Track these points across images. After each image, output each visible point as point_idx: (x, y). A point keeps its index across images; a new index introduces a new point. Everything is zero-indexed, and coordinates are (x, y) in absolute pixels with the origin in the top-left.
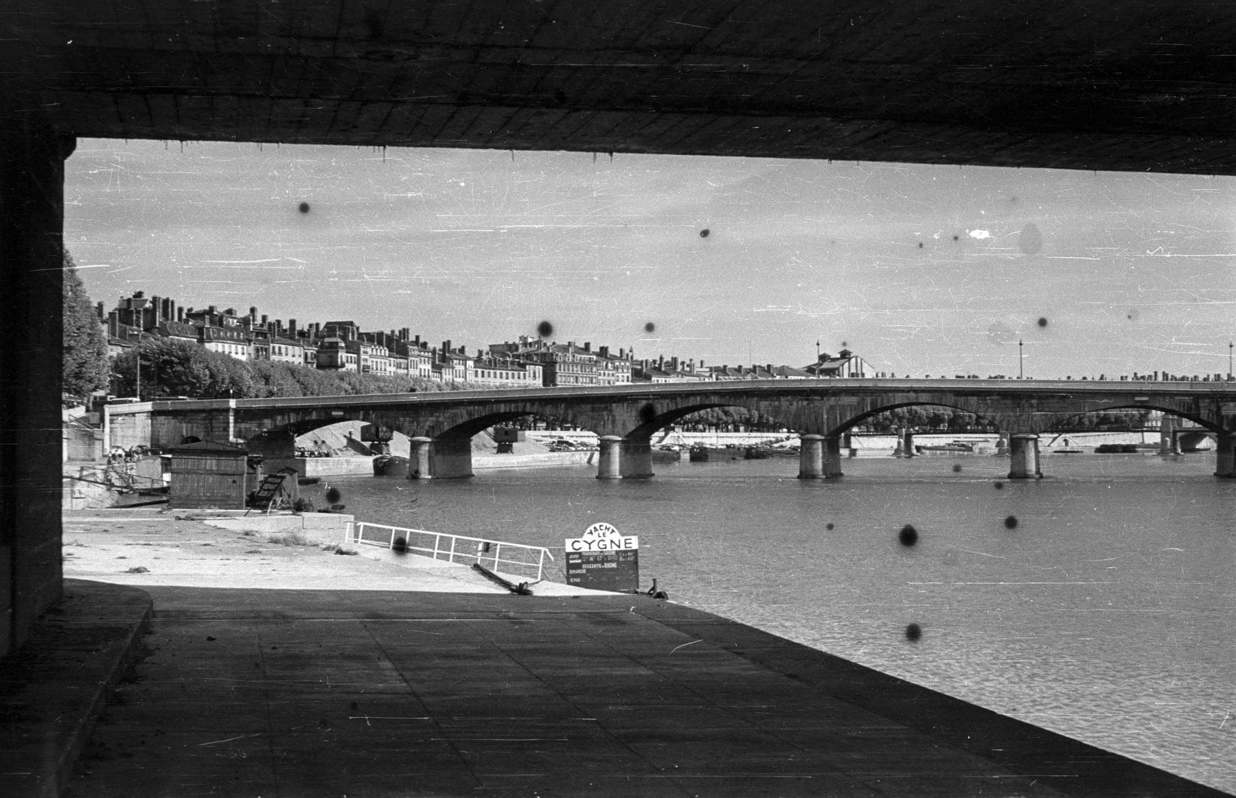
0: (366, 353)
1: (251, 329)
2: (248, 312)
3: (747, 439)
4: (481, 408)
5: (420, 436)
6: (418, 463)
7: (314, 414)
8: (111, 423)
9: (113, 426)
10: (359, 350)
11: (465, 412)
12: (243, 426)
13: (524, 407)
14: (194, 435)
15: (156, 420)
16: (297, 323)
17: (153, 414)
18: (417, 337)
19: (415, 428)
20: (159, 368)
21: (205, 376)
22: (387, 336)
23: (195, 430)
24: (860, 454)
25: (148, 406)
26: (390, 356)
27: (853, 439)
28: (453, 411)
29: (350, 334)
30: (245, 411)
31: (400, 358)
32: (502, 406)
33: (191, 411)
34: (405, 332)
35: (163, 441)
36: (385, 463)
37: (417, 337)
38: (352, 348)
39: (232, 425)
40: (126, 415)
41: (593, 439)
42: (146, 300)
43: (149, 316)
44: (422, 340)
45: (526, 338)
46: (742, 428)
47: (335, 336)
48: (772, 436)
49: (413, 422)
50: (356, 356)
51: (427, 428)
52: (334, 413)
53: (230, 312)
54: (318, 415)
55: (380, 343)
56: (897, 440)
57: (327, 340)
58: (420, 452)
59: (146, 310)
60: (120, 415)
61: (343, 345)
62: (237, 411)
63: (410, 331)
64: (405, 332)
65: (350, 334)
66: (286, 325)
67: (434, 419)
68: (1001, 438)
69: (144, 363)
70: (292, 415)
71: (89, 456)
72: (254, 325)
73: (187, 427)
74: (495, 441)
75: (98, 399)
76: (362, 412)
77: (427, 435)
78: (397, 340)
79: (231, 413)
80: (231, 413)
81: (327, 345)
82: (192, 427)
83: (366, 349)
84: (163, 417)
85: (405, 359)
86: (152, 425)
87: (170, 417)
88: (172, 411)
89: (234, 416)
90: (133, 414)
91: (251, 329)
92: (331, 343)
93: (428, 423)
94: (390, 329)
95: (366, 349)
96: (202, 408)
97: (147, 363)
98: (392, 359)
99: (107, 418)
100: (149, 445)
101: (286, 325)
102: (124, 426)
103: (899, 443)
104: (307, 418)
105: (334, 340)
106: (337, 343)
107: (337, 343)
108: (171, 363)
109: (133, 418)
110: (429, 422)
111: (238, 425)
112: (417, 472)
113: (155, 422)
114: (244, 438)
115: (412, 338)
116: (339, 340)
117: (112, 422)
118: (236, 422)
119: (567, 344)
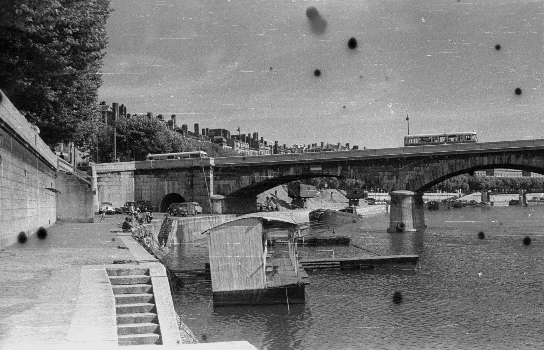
0: (237, 146)
1: (174, 129)
2: (170, 119)
3: (441, 197)
4: (463, 161)
5: (400, 189)
6: (401, 216)
7: (292, 169)
8: (98, 181)
9: (100, 183)
10: (233, 144)
11: (447, 166)
12: (222, 182)
13: (509, 159)
14: (175, 192)
15: (139, 178)
16: (199, 125)
17: (137, 173)
18: (262, 138)
19: (394, 181)
20: (130, 140)
21: (169, 146)
22: (247, 137)
23: (176, 186)
24: (495, 204)
25: (131, 165)
26: (250, 149)
27: (490, 196)
28: (434, 165)
29: (228, 134)
30: (223, 168)
31: (255, 150)
32: (486, 158)
33: (173, 169)
34: (256, 135)
35: (146, 198)
36: (322, 214)
37: (262, 138)
38: (230, 143)
39: (212, 182)
40: (112, 173)
41: (480, 194)
42: (108, 106)
43: (111, 115)
44: (264, 140)
45: (297, 146)
46: (438, 191)
47: (220, 135)
48: (452, 195)
49: (392, 176)
50: (232, 147)
51: (407, 182)
52: (312, 169)
53: (160, 117)
54: (295, 170)
55: (243, 141)
56: (518, 196)
57: (215, 137)
58: (403, 205)
59: (109, 113)
60: (107, 173)
61: (225, 141)
62: (216, 169)
63: (259, 134)
64: (256, 135)
65: (228, 134)
66: (191, 129)
67: (414, 172)
68: (520, 195)
69: (120, 136)
70: (270, 171)
71: (86, 215)
72: (175, 126)
73: (168, 186)
74: (347, 198)
75: (81, 165)
76: (339, 167)
77: (407, 189)
78: (252, 139)
79: (211, 171)
80: (211, 171)
81: (216, 140)
82: (174, 185)
83: (237, 144)
84: (146, 176)
85: (257, 150)
86: (135, 183)
87: (153, 175)
88: (153, 170)
89: (214, 174)
90: (119, 172)
91: (174, 129)
92: (217, 139)
93: (408, 177)
94: (248, 133)
95: (237, 144)
96: (183, 166)
97: (122, 136)
98: (251, 150)
99: (95, 176)
100: (133, 201)
101: (191, 129)
102: (110, 184)
103: (520, 198)
104: (284, 174)
105: (219, 137)
106: (222, 139)
107: (222, 139)
108: (138, 136)
109: (118, 176)
110: (409, 176)
111: (217, 182)
112: (403, 225)
113: (137, 180)
114: (224, 194)
115: (260, 139)
116: (223, 138)
117: (99, 179)
118: (215, 179)
119: (337, 144)
